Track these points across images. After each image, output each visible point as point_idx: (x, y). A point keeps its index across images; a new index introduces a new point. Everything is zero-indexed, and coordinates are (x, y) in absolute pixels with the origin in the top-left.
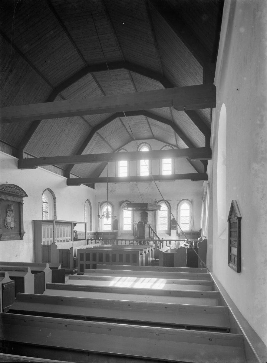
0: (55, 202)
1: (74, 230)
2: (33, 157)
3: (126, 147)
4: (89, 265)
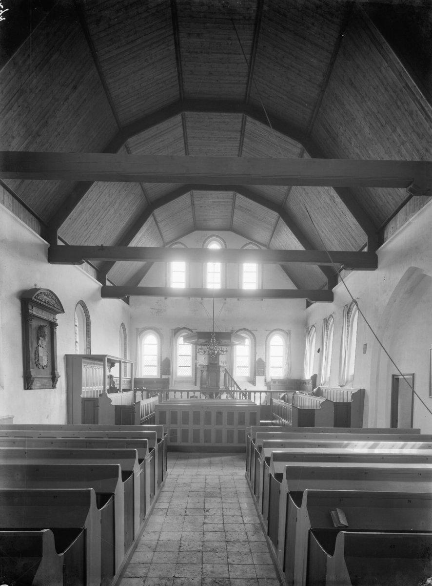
0: (88, 324)
1: (111, 373)
2: (64, 244)
3: (184, 240)
4: (233, 431)
